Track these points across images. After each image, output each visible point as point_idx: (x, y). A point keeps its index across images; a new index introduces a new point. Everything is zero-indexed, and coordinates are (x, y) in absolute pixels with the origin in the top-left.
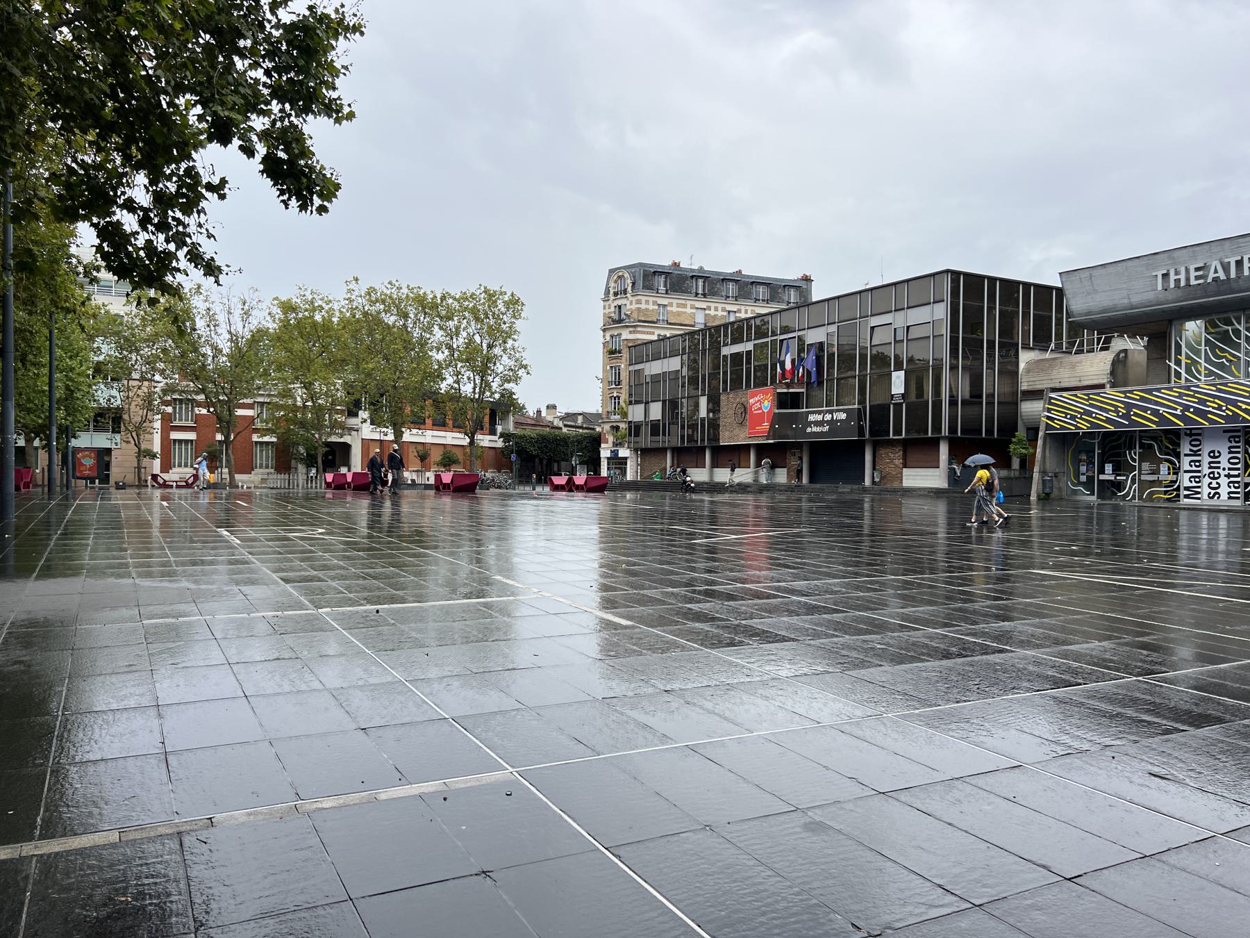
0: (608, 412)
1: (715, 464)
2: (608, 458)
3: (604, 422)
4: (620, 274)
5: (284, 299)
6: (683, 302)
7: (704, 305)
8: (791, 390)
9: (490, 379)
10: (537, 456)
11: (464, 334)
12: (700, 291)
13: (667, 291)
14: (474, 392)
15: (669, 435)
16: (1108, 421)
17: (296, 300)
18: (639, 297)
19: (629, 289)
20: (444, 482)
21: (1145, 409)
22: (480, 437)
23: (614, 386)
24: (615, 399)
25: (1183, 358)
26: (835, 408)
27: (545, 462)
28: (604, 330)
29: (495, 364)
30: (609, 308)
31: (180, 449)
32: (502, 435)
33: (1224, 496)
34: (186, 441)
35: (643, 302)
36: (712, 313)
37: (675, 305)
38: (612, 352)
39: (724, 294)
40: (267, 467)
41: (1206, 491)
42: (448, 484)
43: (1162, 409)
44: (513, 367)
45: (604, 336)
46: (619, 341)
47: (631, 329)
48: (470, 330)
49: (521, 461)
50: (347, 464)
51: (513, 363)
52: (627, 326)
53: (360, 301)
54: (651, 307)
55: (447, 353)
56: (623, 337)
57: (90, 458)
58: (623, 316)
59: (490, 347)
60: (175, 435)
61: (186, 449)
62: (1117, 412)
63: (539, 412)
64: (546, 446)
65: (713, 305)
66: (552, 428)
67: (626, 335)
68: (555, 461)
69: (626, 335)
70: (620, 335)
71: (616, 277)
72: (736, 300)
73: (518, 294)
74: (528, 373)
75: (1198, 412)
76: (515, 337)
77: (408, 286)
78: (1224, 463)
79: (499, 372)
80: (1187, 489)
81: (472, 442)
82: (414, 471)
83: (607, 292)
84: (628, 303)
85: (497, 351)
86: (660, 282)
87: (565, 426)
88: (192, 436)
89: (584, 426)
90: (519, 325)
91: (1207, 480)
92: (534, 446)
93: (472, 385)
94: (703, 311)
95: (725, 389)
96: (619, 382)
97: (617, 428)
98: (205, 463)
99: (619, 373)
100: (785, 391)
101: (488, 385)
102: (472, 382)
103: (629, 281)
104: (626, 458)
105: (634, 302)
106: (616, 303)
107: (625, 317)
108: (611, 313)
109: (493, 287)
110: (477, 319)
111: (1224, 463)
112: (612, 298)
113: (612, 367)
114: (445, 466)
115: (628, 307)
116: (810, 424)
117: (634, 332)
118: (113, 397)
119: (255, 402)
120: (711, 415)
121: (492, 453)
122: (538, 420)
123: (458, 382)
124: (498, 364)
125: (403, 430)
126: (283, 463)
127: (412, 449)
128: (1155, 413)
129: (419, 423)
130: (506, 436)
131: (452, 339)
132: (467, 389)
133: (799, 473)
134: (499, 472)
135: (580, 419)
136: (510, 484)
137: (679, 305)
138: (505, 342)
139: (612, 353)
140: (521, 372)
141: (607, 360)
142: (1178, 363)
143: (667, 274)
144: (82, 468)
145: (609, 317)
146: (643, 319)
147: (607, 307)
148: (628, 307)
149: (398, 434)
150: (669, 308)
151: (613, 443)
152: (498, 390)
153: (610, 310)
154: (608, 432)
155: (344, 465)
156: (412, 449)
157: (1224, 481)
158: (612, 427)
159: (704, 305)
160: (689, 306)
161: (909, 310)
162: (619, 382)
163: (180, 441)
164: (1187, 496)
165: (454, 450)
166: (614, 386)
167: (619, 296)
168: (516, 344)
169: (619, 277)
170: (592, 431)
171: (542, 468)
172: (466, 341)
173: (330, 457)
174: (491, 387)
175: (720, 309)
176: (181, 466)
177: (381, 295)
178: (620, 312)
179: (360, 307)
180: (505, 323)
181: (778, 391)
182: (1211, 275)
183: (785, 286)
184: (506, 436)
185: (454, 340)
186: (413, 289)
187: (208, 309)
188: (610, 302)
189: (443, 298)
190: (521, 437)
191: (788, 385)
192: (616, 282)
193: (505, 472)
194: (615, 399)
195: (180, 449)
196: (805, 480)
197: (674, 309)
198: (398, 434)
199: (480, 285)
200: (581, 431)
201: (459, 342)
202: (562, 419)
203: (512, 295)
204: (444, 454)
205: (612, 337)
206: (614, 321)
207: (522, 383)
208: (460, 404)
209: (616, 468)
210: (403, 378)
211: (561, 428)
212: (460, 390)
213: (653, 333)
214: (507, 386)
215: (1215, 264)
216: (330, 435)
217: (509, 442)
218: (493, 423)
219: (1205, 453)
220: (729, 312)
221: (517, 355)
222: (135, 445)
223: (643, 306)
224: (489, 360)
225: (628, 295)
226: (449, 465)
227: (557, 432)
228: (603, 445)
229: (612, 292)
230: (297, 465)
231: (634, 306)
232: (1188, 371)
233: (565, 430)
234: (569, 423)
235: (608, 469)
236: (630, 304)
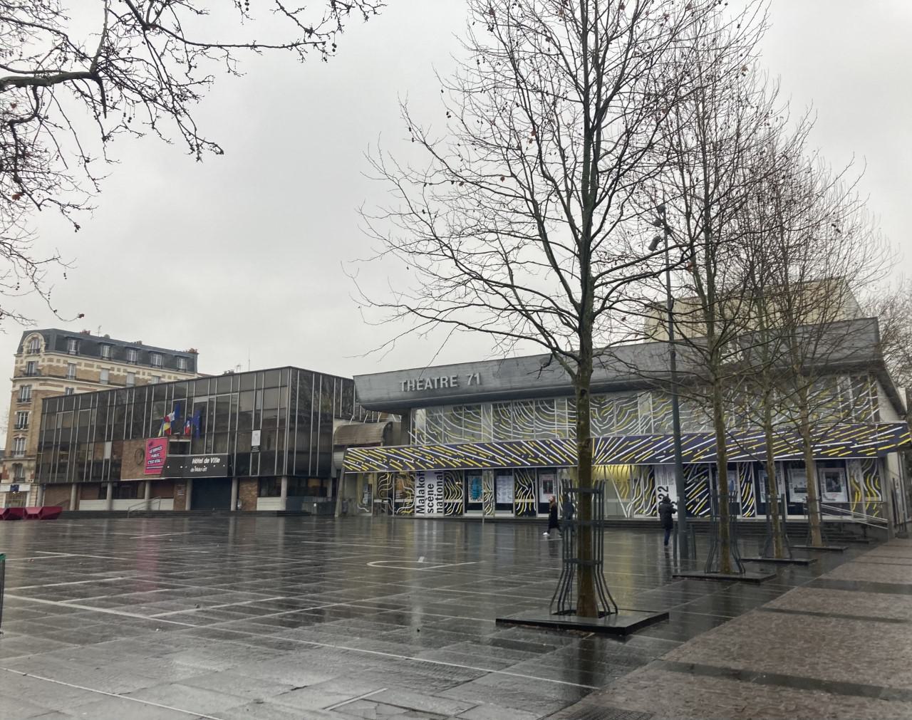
6: (91, 363)
8: (181, 441)
16: (378, 466)
19: (43, 349)
21: (396, 460)
25: (416, 430)
30: (22, 362)
33: (435, 511)
41: (427, 508)
43: (405, 460)
47: (42, 382)
62: (382, 461)
70: (30, 386)
75: (422, 462)
78: (435, 489)
80: (418, 507)
84: (40, 360)
91: (427, 502)
100: (176, 441)
105: (46, 360)
111: (435, 489)
117: (44, 384)
128: (401, 462)
137: (86, 365)
142: (414, 433)
148: (40, 363)
157: (435, 502)
164: (418, 512)
169: (34, 339)
181: (171, 440)
182: (426, 386)
192: (30, 342)
197: (83, 368)
213: (62, 386)
215: (428, 380)
219: (426, 486)
223: (54, 364)
231: (46, 363)
232: (419, 439)
236: (43, 361)
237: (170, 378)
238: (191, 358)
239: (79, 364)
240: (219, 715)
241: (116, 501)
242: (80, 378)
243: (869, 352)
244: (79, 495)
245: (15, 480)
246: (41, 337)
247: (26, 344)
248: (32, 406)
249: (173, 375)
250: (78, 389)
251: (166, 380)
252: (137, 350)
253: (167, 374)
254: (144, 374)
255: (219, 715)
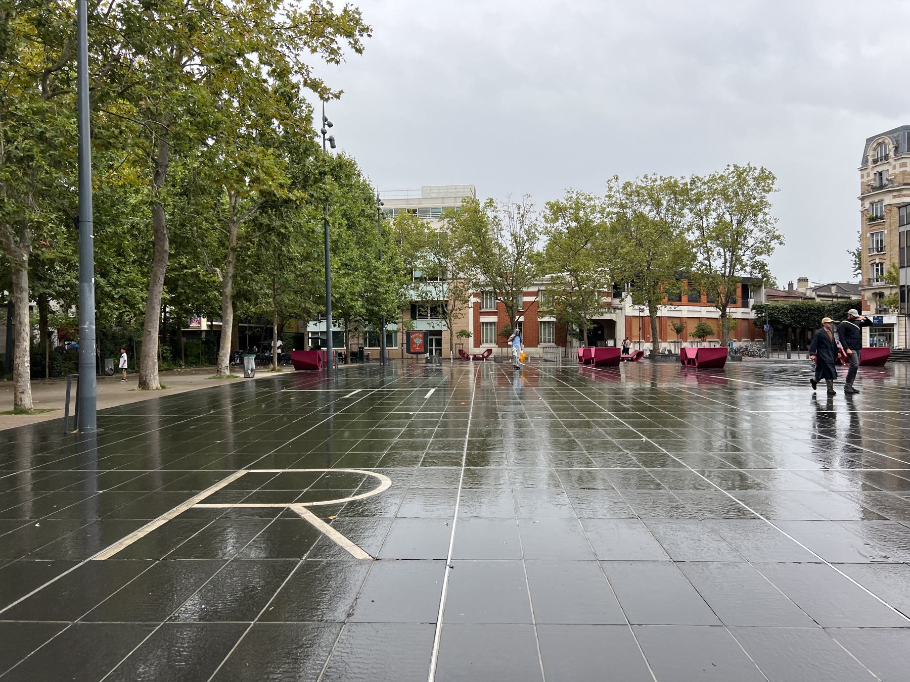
0: (869, 279)
3: (864, 290)
4: (880, 141)
5: (553, 201)
9: (741, 253)
10: (790, 325)
11: (714, 215)
14: (725, 267)
15: (908, 302)
17: (563, 201)
19: (892, 154)
20: (688, 357)
22: (733, 310)
23: (876, 253)
24: (877, 265)
27: (798, 331)
28: (862, 199)
29: (745, 238)
30: (868, 176)
31: (487, 329)
32: (754, 308)
34: (491, 323)
38: (872, 219)
40: (549, 342)
42: (693, 360)
44: (764, 239)
45: (862, 205)
46: (881, 208)
47: (895, 194)
48: (720, 211)
49: (774, 331)
50: (613, 337)
51: (765, 234)
52: (890, 191)
53: (618, 196)
55: (697, 233)
56: (886, 202)
57: (419, 338)
58: (885, 182)
59: (740, 223)
60: (483, 319)
61: (491, 329)
63: (791, 285)
64: (799, 316)
66: (805, 298)
67: (888, 200)
68: (809, 330)
69: (888, 200)
70: (881, 201)
71: (875, 144)
73: (769, 168)
74: (781, 243)
76: (766, 210)
77: (661, 177)
79: (750, 245)
81: (724, 315)
82: (672, 342)
83: (865, 161)
85: (748, 225)
87: (818, 296)
88: (494, 319)
89: (839, 295)
90: (769, 197)
92: (787, 315)
93: (723, 260)
96: (882, 248)
97: (881, 295)
98: (518, 339)
101: (739, 260)
102: (723, 258)
103: (891, 146)
104: (892, 325)
105: (898, 166)
106: (875, 170)
107: (887, 182)
108: (871, 180)
109: (743, 164)
110: (727, 199)
112: (870, 165)
113: (872, 234)
114: (700, 337)
115: (891, 172)
117: (899, 196)
118: (430, 292)
119: (539, 290)
121: (745, 324)
122: (790, 294)
123: (708, 259)
124: (749, 239)
125: (659, 306)
126: (561, 339)
127: (669, 322)
129: (676, 299)
130: (758, 308)
131: (702, 218)
132: (717, 264)
134: (753, 340)
135: (834, 289)
136: (763, 353)
138: (755, 215)
139: (873, 219)
140: (773, 244)
141: (867, 228)
144: (414, 346)
145: (868, 185)
147: (865, 176)
148: (891, 172)
149: (653, 310)
151: (877, 310)
152: (749, 262)
153: (869, 178)
154: (869, 299)
156: (669, 322)
158: (875, 294)
161: (908, 268)
162: (882, 248)
163: (487, 323)
165: (709, 323)
166: (876, 253)
167: (879, 163)
168: (768, 217)
169: (879, 144)
170: (849, 300)
171: (795, 336)
172: (717, 220)
173: (599, 332)
174: (742, 260)
177: (636, 187)
178: (881, 179)
179: (618, 202)
180: (754, 199)
184: (758, 308)
185: (704, 220)
186: (665, 179)
187: (495, 217)
189: (693, 182)
190: (773, 308)
193: (758, 341)
194: (877, 265)
195: (487, 329)
198: (653, 310)
199: (728, 166)
200: (835, 300)
201: (710, 221)
202: (815, 290)
203: (763, 170)
204: (699, 326)
205: (872, 204)
206: (874, 189)
207: (774, 254)
208: (711, 279)
209: (879, 335)
210: (655, 259)
211: (814, 299)
212: (710, 266)
214: (758, 258)
216: (592, 314)
217: (761, 314)
218: (745, 296)
221: (769, 227)
222: (448, 327)
224: (739, 234)
225: (890, 160)
226: (704, 336)
227: (810, 302)
229: (870, 160)
230: (572, 340)
231: (898, 170)
233: (818, 300)
234: (823, 294)
235: (871, 336)
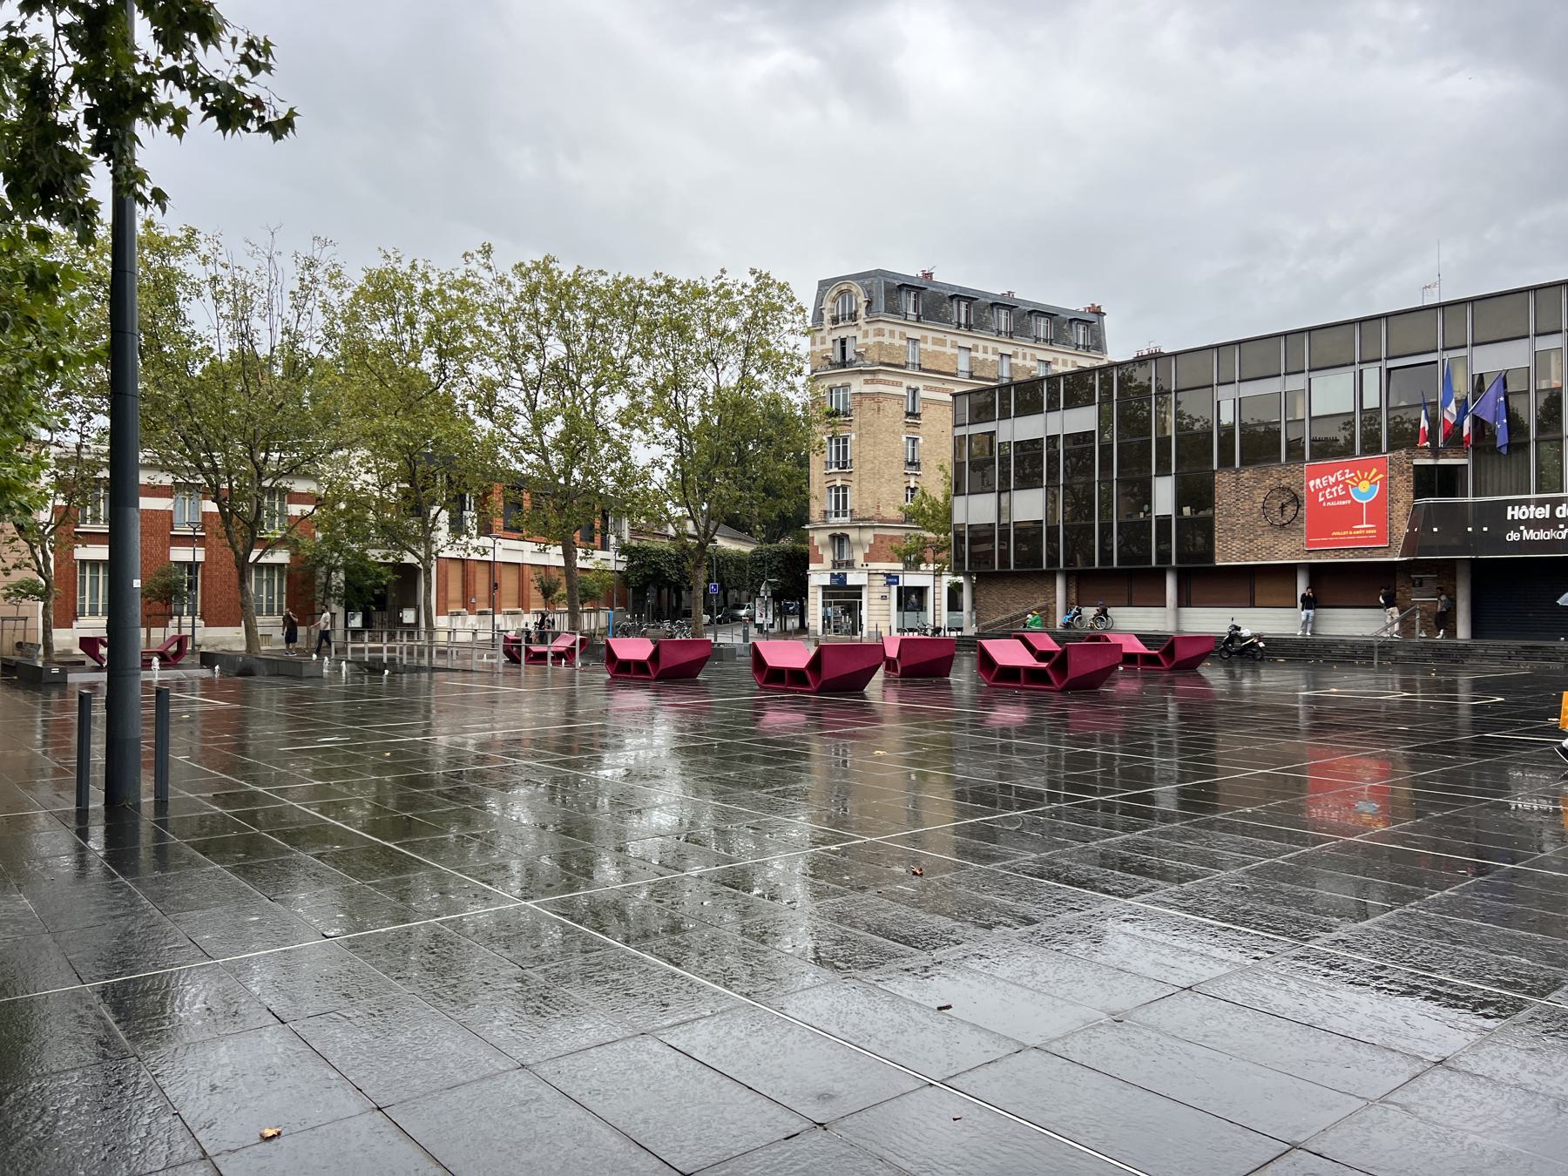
0: (826, 512)
1: (1184, 601)
2: (824, 587)
4: (844, 287)
6: (940, 336)
7: (968, 343)
8: (1442, 462)
12: (963, 321)
13: (918, 318)
18: (881, 325)
19: (862, 311)
20: (888, 655)
26: (1533, 496)
30: (823, 343)
35: (887, 334)
36: (980, 355)
37: (930, 340)
39: (994, 328)
46: (845, 397)
47: (868, 377)
52: (861, 372)
54: (898, 342)
56: (854, 389)
58: (850, 355)
65: (981, 344)
70: (846, 386)
71: (835, 292)
72: (1011, 338)
84: (859, 335)
86: (908, 302)
94: (967, 352)
95: (1226, 461)
99: (845, 448)
100: (1430, 462)
103: (862, 299)
104: (860, 587)
105: (871, 333)
108: (827, 350)
112: (827, 326)
116: (1515, 524)
117: (872, 382)
120: (1187, 510)
133: (1445, 620)
137: (936, 342)
143: (918, 290)
145: (826, 358)
146: (886, 361)
148: (860, 340)
150: (922, 345)
151: (834, 562)
153: (824, 347)
154: (823, 545)
155: (409, 606)
158: (833, 537)
159: (968, 343)
160: (949, 343)
162: (845, 463)
166: (836, 470)
167: (841, 324)
169: (841, 293)
175: (990, 351)
176: (96, 614)
181: (1416, 462)
183: (1071, 320)
184: (624, 550)
188: (824, 333)
191: (1436, 453)
192: (834, 300)
196: (1463, 632)
197: (929, 347)
198: (568, 555)
209: (836, 603)
213: (900, 384)
220: (1002, 355)
223: (886, 340)
228: (812, 566)
231: (871, 340)
236: (863, 337)
237: (1065, 363)
238: (1090, 323)
239: (925, 339)
240: (931, 1170)
241: (1184, 610)
242: (927, 367)
243: (982, 587)
244: (1073, 596)
245: (836, 565)
246: (856, 288)
247: (828, 305)
248: (855, 426)
249: (1070, 358)
250: (927, 388)
251: (1059, 368)
252: (1010, 308)
253: (1061, 357)
254: (1024, 357)
255: (931, 1170)
